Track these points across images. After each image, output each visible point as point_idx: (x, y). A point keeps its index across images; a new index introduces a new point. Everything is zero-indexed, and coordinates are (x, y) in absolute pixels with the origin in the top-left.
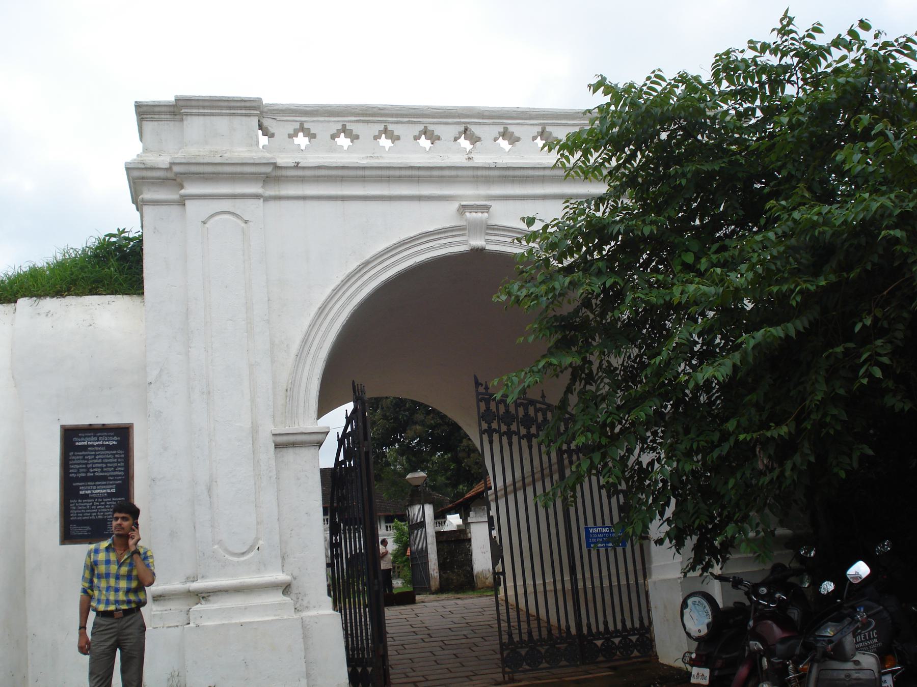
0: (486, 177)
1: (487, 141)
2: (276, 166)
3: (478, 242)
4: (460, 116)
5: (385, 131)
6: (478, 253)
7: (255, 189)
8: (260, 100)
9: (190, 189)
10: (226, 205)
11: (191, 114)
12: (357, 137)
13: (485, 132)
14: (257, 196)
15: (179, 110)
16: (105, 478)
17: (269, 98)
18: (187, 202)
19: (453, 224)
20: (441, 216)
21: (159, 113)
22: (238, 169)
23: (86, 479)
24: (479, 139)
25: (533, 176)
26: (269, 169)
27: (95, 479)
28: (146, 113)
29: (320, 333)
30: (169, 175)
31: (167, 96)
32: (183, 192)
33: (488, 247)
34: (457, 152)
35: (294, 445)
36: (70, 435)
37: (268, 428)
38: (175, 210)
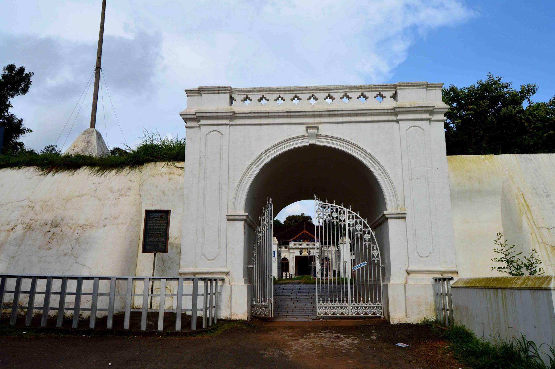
0: (318, 115)
1: (321, 100)
2: (234, 113)
3: (312, 141)
4: (310, 90)
5: (346, 95)
6: (312, 146)
7: (227, 121)
8: (231, 87)
9: (203, 122)
10: (215, 128)
11: (363, 92)
12: (351, 98)
13: (337, 95)
14: (226, 124)
15: (200, 91)
16: (159, 229)
17: (234, 86)
18: (400, 122)
19: (303, 134)
20: (300, 130)
21: (194, 93)
22: (356, 112)
23: (153, 229)
24: (385, 97)
25: (338, 114)
26: (231, 114)
27: (156, 229)
28: (189, 92)
29: (247, 177)
30: (195, 117)
31: (196, 87)
32: (200, 123)
33: (317, 143)
34: (305, 104)
35: (234, 220)
36: (148, 212)
37: (225, 213)
38: (198, 129)
